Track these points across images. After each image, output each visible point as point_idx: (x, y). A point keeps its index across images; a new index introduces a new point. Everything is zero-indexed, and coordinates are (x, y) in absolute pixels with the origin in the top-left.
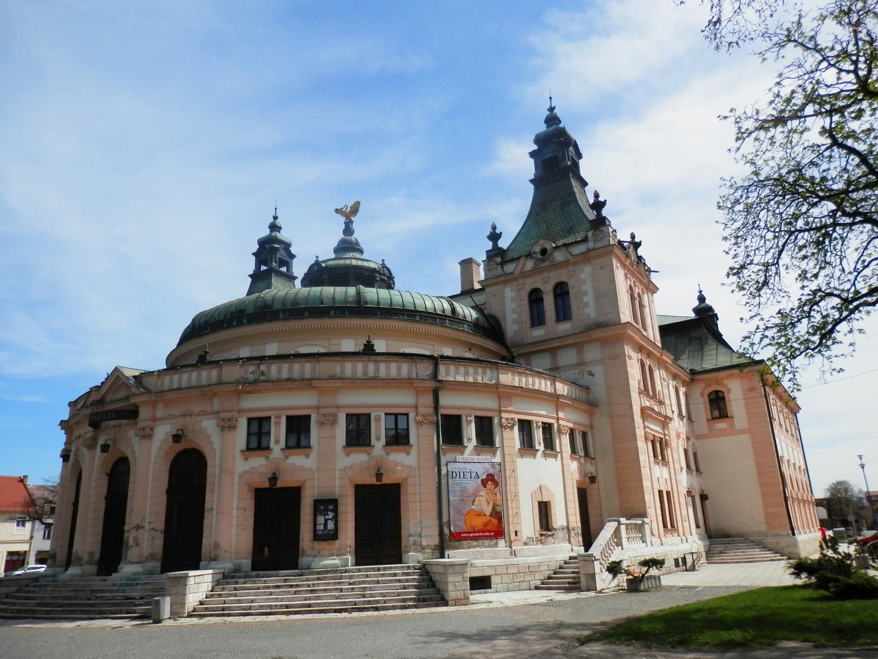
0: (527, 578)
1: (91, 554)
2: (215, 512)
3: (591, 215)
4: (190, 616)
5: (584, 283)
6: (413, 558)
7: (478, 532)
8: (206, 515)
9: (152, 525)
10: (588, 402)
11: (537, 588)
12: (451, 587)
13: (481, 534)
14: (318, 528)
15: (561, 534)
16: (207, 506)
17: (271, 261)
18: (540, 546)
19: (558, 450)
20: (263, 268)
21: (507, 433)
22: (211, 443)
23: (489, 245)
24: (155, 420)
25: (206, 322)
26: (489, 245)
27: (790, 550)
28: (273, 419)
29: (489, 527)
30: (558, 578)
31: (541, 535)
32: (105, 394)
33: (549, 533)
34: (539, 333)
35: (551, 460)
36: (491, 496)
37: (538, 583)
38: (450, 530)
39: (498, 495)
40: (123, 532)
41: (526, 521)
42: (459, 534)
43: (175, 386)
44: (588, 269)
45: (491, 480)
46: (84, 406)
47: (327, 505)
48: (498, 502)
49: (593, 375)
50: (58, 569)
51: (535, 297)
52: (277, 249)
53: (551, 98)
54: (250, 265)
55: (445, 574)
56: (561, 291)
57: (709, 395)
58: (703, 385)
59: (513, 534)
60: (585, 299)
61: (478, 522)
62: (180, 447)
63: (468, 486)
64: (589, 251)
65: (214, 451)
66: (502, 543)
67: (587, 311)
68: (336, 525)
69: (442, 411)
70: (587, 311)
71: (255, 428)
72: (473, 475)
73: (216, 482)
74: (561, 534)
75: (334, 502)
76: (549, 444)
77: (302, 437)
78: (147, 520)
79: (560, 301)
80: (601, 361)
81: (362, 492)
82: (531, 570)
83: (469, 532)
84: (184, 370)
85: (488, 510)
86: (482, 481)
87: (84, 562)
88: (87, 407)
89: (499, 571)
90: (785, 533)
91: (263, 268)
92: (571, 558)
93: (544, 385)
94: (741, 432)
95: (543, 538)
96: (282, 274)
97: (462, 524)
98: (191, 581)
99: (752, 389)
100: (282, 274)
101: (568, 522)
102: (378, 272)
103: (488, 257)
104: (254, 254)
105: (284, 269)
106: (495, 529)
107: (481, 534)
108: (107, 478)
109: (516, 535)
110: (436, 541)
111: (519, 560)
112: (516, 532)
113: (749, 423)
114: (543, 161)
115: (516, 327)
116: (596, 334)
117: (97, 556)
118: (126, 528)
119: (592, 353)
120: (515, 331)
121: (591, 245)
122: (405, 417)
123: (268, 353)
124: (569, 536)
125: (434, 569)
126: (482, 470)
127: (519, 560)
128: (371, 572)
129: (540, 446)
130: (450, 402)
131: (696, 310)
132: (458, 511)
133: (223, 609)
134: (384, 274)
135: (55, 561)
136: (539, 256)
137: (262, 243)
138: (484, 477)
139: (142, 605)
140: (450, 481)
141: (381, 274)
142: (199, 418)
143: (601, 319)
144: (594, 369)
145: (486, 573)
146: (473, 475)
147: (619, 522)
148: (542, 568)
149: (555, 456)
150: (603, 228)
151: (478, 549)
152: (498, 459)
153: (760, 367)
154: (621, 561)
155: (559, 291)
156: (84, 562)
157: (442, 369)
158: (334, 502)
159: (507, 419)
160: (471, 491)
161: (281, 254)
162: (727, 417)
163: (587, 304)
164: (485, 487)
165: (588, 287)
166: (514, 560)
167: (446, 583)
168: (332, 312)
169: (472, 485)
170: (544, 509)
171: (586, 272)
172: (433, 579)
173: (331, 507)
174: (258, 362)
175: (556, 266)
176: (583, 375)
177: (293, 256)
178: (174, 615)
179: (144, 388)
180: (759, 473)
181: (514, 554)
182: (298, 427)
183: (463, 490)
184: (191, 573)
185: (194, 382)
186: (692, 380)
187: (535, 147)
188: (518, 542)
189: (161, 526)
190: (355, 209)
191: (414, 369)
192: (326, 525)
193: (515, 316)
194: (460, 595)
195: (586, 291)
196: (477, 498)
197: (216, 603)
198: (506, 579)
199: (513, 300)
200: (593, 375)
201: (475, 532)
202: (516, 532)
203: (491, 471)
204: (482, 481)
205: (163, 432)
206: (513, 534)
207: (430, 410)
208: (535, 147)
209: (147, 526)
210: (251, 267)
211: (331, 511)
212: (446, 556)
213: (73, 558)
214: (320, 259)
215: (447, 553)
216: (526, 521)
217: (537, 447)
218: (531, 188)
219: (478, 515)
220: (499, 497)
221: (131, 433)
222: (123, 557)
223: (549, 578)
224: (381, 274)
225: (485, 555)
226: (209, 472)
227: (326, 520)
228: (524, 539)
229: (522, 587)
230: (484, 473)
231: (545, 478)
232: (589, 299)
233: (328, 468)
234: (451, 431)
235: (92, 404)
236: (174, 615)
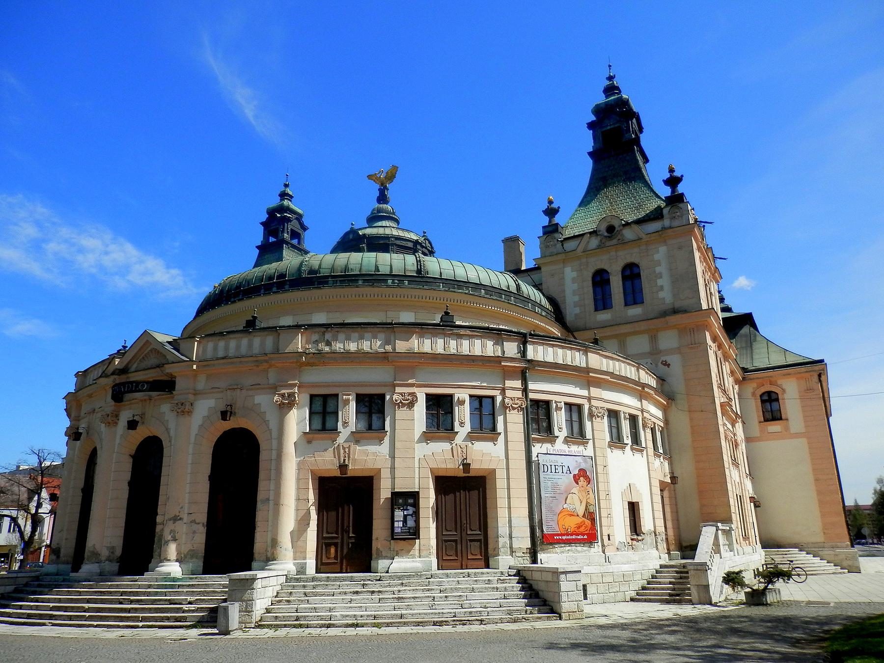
1: (112, 549)
2: (271, 503)
3: (666, 191)
4: (259, 626)
5: (659, 263)
6: (505, 561)
7: (572, 535)
8: (259, 505)
9: (192, 517)
10: (667, 393)
11: (632, 600)
12: (564, 597)
13: (574, 537)
14: (396, 524)
15: (649, 539)
16: (261, 496)
17: (283, 232)
18: (631, 552)
19: (644, 445)
20: (272, 239)
21: (597, 421)
22: (266, 422)
23: (545, 221)
24: (197, 393)
25: (222, 291)
26: (545, 221)
27: (850, 563)
29: (582, 529)
30: (654, 589)
31: (632, 539)
32: (129, 362)
33: (640, 538)
34: (604, 316)
35: (638, 455)
36: (584, 494)
37: (633, 594)
38: (542, 531)
39: (591, 492)
40: (154, 524)
41: (616, 524)
43: (221, 354)
44: (663, 249)
46: (104, 375)
47: (408, 499)
48: (592, 501)
49: (669, 365)
50: (62, 567)
51: (600, 279)
52: (289, 220)
53: (610, 66)
54: (258, 236)
55: (557, 582)
56: (631, 273)
57: (761, 396)
58: (754, 385)
59: (606, 538)
60: (660, 282)
61: (571, 523)
62: (228, 425)
63: (560, 482)
64: (664, 229)
65: (270, 431)
66: (597, 548)
67: (661, 295)
68: (417, 521)
69: (532, 396)
70: (661, 295)
71: (318, 406)
73: (273, 468)
74: (649, 539)
75: (415, 496)
76: (636, 440)
77: (374, 417)
78: (186, 511)
79: (629, 284)
80: (679, 350)
81: (445, 484)
82: (625, 578)
84: (232, 336)
85: (581, 510)
86: (575, 476)
88: (107, 376)
89: (595, 580)
90: (844, 545)
91: (272, 239)
92: (661, 566)
93: (627, 370)
94: (797, 435)
95: (634, 542)
96: (293, 246)
97: (554, 525)
98: (258, 584)
99: (810, 390)
100: (293, 246)
101: (655, 527)
102: (420, 244)
103: (544, 233)
104: (262, 223)
105: (295, 242)
106: (588, 534)
107: (574, 537)
108: (131, 460)
110: (527, 544)
113: (806, 427)
114: (603, 133)
115: (577, 310)
116: (673, 319)
117: (119, 552)
118: (159, 519)
119: (668, 340)
120: (576, 315)
121: (666, 222)
122: (490, 400)
123: (314, 322)
124: (656, 542)
125: (537, 576)
126: (574, 465)
128: (455, 578)
129: (628, 440)
130: (540, 388)
132: (551, 510)
133: (297, 619)
134: (426, 248)
135: (58, 557)
136: (606, 234)
137: (271, 212)
139: (193, 611)
141: (423, 247)
142: (251, 393)
143: (678, 305)
144: (668, 359)
146: (565, 469)
147: (717, 527)
149: (642, 451)
150: (681, 205)
151: (571, 554)
152: (589, 451)
153: (817, 367)
154: (741, 572)
155: (628, 273)
156: (103, 559)
157: (530, 348)
158: (415, 496)
159: (597, 408)
160: (563, 488)
161: (294, 225)
162: (781, 419)
163: (662, 288)
165: (662, 269)
167: (558, 593)
168: (390, 282)
170: (633, 508)
171: (661, 253)
172: (535, 587)
173: (411, 501)
174: (323, 330)
175: (624, 243)
176: (657, 365)
177: (304, 228)
178: (244, 625)
180: (816, 480)
181: (607, 560)
182: (373, 407)
183: (555, 487)
184: (260, 574)
185: (244, 350)
186: (744, 378)
187: (593, 118)
189: (203, 517)
190: (391, 177)
191: (499, 348)
192: (405, 521)
193: (576, 298)
194: (573, 607)
195: (661, 273)
197: (285, 611)
198: (602, 588)
199: (574, 280)
200: (669, 365)
201: (568, 535)
203: (583, 466)
205: (205, 407)
206: (606, 538)
207: (519, 394)
208: (593, 118)
209: (186, 518)
210: (259, 239)
211: (411, 505)
212: (539, 561)
213: (87, 554)
214: (356, 227)
216: (616, 524)
217: (556, 433)
218: (589, 163)
221: (165, 408)
222: (155, 554)
223: (644, 588)
224: (423, 247)
226: (263, 456)
227: (405, 517)
229: (618, 599)
230: (576, 468)
231: (633, 475)
232: (664, 281)
233: (408, 457)
234: (539, 415)
235: (113, 374)
236: (244, 625)
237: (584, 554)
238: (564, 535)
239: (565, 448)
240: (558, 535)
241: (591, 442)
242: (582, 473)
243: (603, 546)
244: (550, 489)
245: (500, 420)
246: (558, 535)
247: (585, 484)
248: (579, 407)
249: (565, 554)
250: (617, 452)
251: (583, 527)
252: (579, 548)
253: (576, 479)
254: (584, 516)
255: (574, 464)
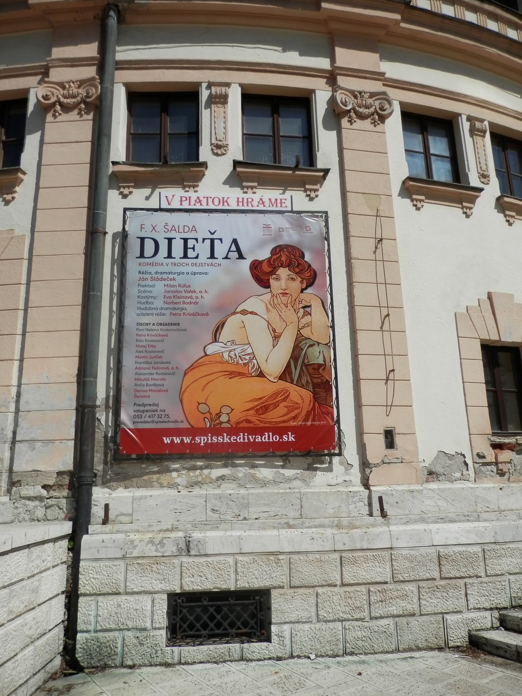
0: (433, 603)
7: (233, 431)
28: (204, 94)
29: (276, 415)
31: (496, 446)
36: (289, 314)
39: (316, 309)
42: (151, 436)
45: (289, 265)
59: (375, 446)
61: (235, 398)
63: (198, 283)
72: (221, 250)
83: (193, 432)
85: (274, 359)
87: (352, 111)
89: (307, 572)
95: (506, 455)
109: (390, 444)
111: (398, 533)
112: (389, 437)
126: (257, 239)
127: (398, 533)
131: (15, 192)
132: (153, 357)
138: (264, 254)
140: (133, 265)
145: (251, 580)
148: (497, 566)
160: (208, 299)
164: (265, 284)
166: (381, 534)
169: (216, 279)
179: (238, 313)
183: (178, 298)
188: (398, 470)
196: (233, 322)
198: (335, 602)
201: (217, 431)
202: (389, 437)
203: (290, 237)
204: (256, 267)
215: (99, 495)
219: (232, 374)
220: (317, 314)
225: (254, 512)
228: (426, 456)
229: (407, 639)
230: (262, 244)
237: (282, 489)
238: (203, 432)
239: (234, 196)
240: (178, 432)
241: (333, 177)
242: (288, 257)
243: (365, 464)
244: (159, 303)
245: (31, 142)
246: (178, 432)
247: (297, 285)
248: (303, 102)
249: (211, 491)
250: (440, 215)
251: (281, 410)
252: (265, 473)
253: (262, 274)
254: (285, 375)
255: (258, 233)
